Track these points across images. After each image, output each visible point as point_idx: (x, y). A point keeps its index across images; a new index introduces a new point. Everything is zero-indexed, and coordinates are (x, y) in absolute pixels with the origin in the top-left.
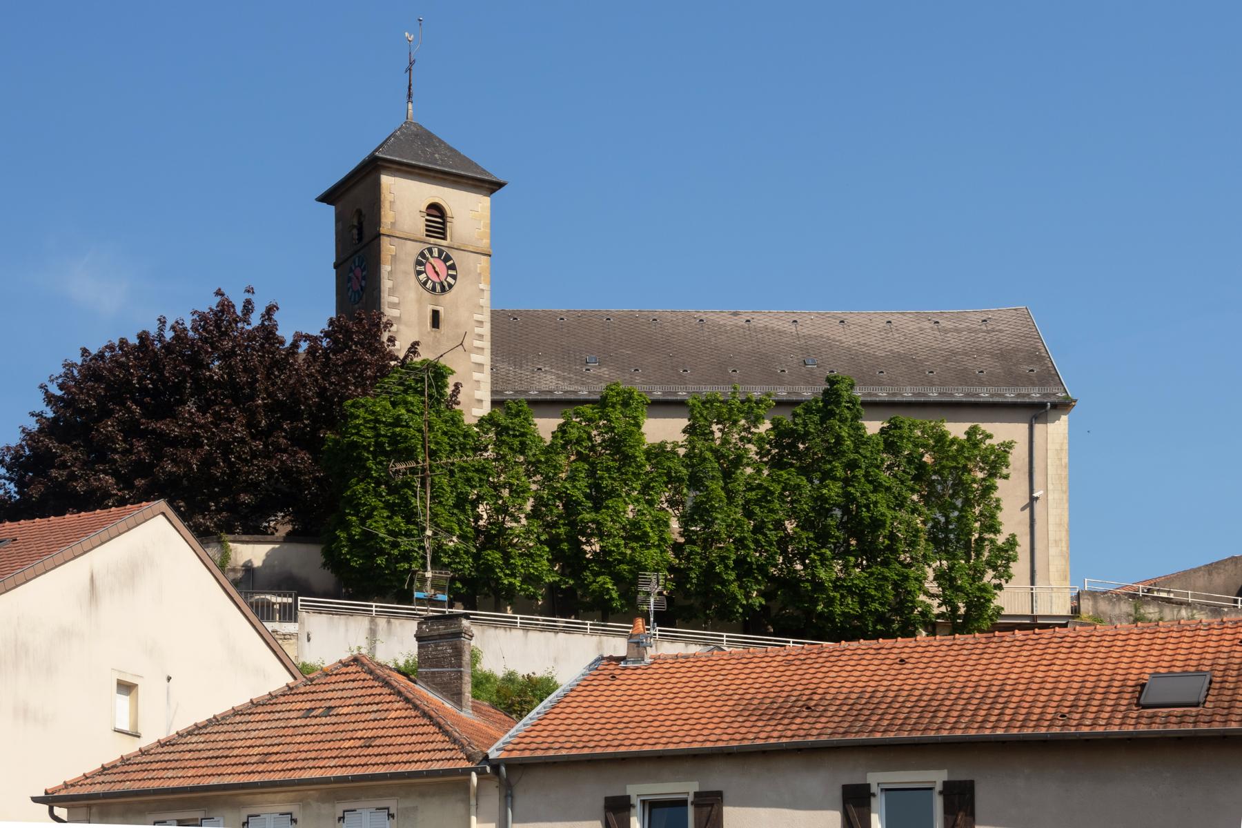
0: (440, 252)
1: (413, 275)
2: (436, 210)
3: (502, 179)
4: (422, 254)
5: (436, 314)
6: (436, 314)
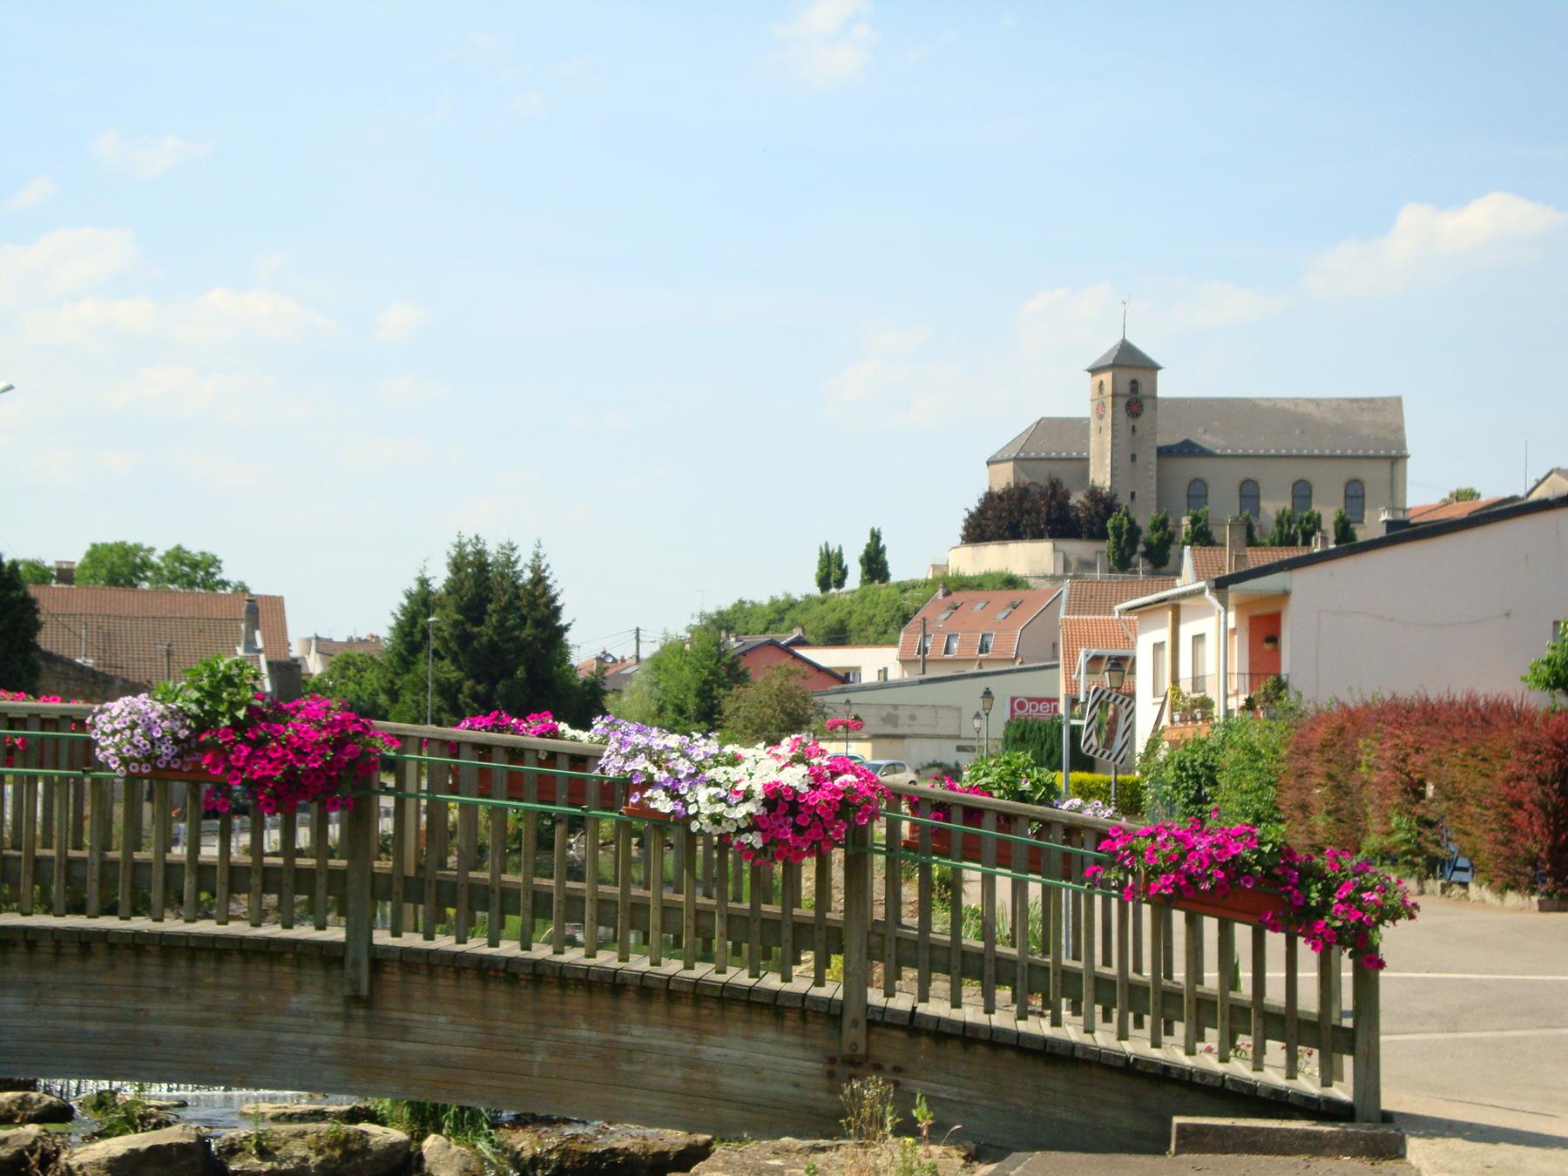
4: (1129, 402)
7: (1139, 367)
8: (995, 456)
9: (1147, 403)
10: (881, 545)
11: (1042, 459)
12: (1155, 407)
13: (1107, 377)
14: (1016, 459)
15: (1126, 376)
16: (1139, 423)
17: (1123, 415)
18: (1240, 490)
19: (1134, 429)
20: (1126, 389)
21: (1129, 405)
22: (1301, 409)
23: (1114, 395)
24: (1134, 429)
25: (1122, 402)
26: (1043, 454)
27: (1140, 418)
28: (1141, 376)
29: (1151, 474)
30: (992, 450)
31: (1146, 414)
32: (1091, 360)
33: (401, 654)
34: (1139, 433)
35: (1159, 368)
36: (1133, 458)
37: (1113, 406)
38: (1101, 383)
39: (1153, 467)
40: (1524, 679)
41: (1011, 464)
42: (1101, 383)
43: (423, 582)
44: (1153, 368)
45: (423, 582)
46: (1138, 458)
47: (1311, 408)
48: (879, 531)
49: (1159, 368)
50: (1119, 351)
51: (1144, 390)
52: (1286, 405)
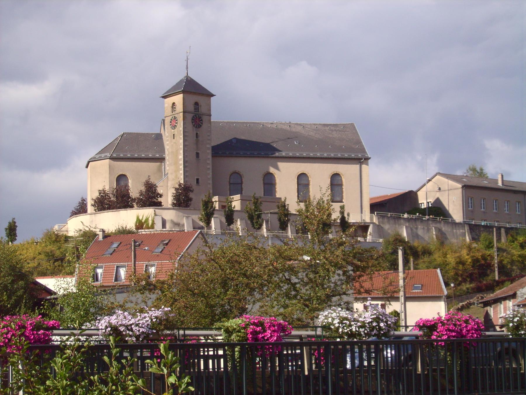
0: (198, 116)
1: (191, 123)
3: (214, 94)
4: (193, 117)
5: (197, 134)
6: (197, 134)
9: (205, 118)
17: (190, 126)
18: (264, 180)
20: (191, 108)
22: (294, 130)
23: (184, 112)
25: (190, 116)
29: (208, 167)
31: (205, 126)
34: (200, 138)
35: (213, 95)
36: (197, 154)
37: (184, 120)
38: (174, 103)
39: (210, 162)
42: (174, 103)
46: (200, 155)
47: (299, 129)
49: (213, 95)
52: (284, 127)
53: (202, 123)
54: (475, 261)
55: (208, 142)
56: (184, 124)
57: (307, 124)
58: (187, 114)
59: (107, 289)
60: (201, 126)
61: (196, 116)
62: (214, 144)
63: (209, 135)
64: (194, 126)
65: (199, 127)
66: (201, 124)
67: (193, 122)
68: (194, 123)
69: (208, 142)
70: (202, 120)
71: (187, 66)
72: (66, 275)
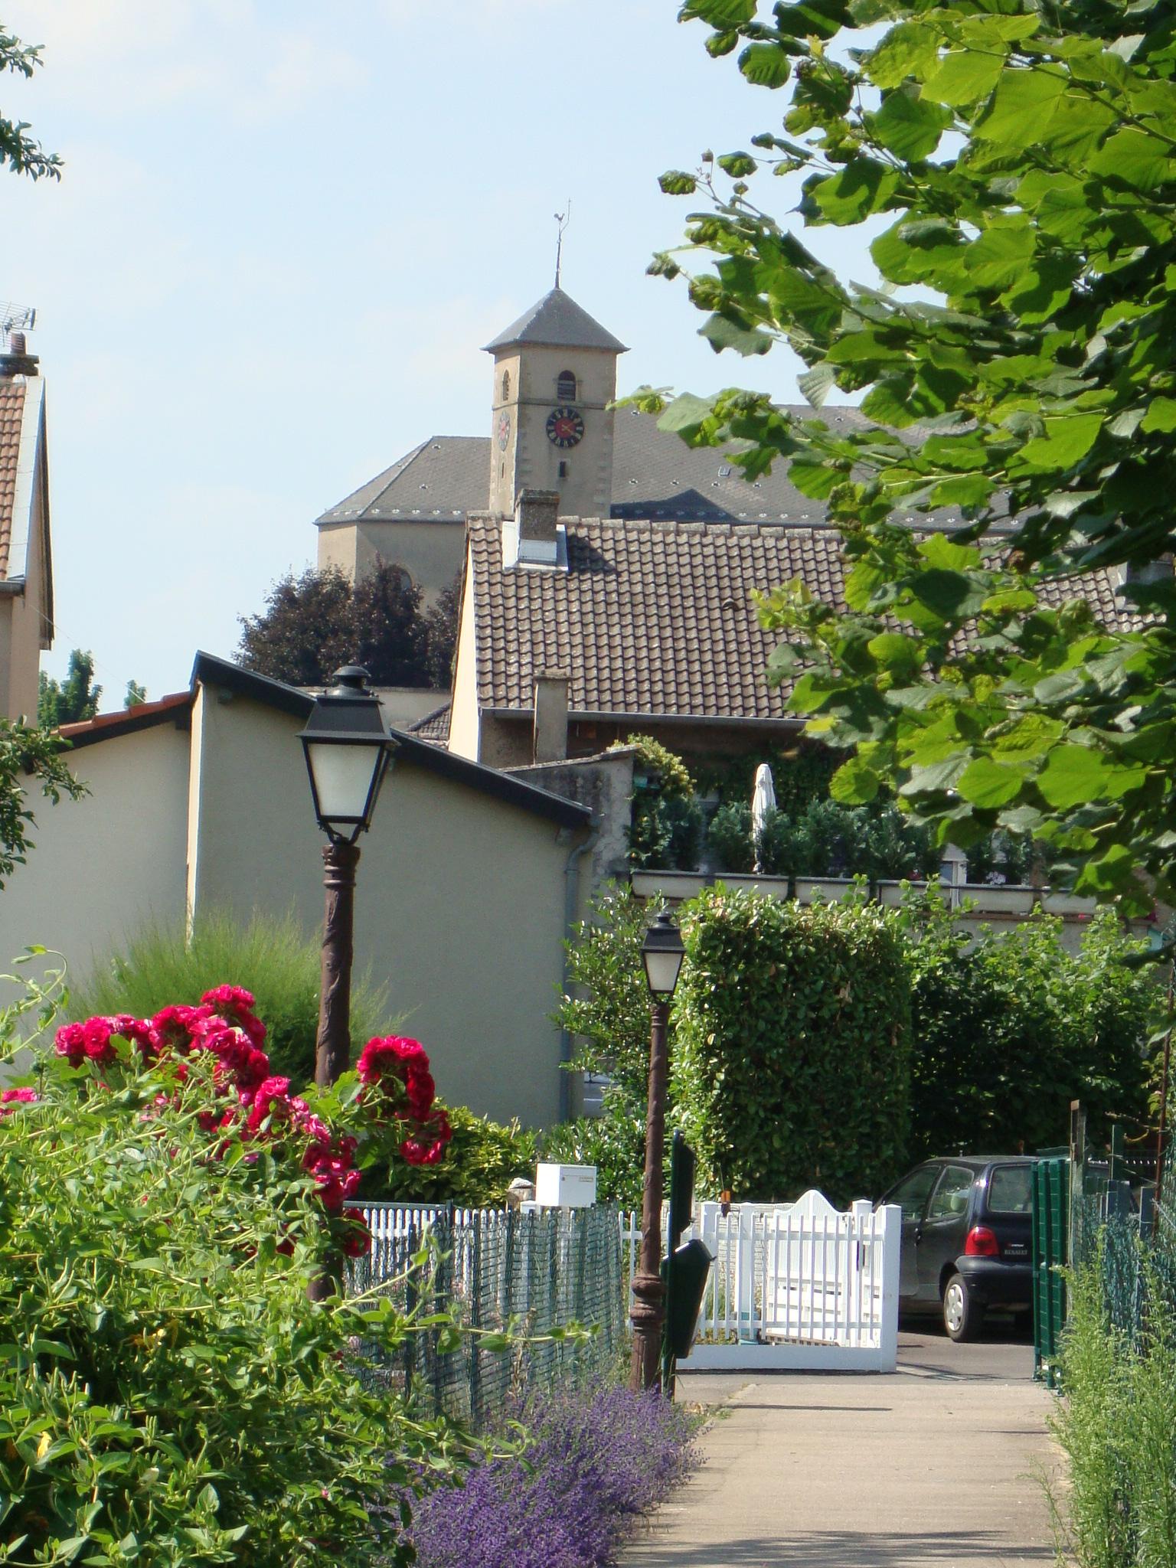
0: (570, 412)
1: (545, 434)
2: (567, 376)
4: (553, 416)
5: (563, 466)
6: (563, 466)
7: (574, 348)
8: (330, 513)
9: (591, 419)
10: (91, 686)
11: (434, 523)
12: (609, 426)
13: (513, 364)
14: (362, 522)
15: (553, 364)
16: (573, 457)
19: (563, 471)
20: (548, 389)
21: (553, 423)
23: (523, 403)
24: (563, 471)
25: (541, 416)
26: (416, 513)
27: (575, 449)
28: (582, 366)
30: (327, 502)
31: (591, 440)
32: (492, 337)
33: (13, 45)
34: (573, 477)
35: (622, 349)
37: (520, 425)
38: (507, 374)
40: (29, 815)
41: (352, 531)
42: (507, 374)
43: (742, 477)
44: (612, 349)
45: (742, 477)
48: (89, 662)
49: (622, 349)
50: (539, 314)
51: (587, 392)
53: (581, 433)
54: (317, 1261)
55: (601, 486)
56: (521, 436)
57: (847, 408)
58: (531, 411)
59: (842, 1299)
60: (577, 441)
61: (561, 412)
62: (614, 502)
63: (603, 469)
64: (553, 441)
65: (570, 445)
66: (578, 436)
67: (549, 432)
68: (553, 435)
69: (601, 486)
70: (581, 424)
71: (345, 889)
72: (902, 1174)
